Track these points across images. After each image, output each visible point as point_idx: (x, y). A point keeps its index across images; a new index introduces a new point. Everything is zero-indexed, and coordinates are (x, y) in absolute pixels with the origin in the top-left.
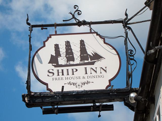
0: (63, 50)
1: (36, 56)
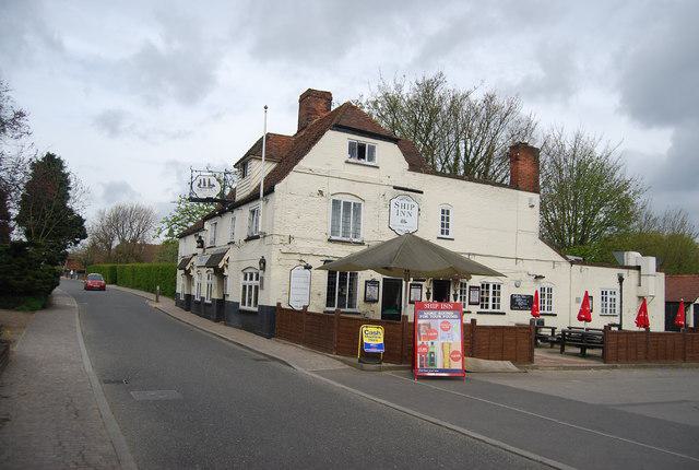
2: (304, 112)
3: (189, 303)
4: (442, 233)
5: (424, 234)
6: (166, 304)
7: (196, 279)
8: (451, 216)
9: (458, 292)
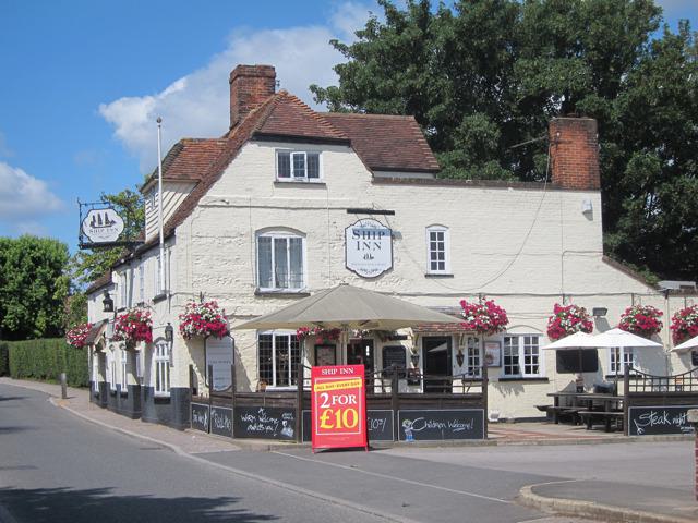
0: (97, 219)
1: (184, 79)
2: (237, 100)
3: (106, 397)
4: (434, 266)
5: (154, 332)
6: (78, 405)
7: (110, 357)
8: (447, 241)
9: (465, 353)
